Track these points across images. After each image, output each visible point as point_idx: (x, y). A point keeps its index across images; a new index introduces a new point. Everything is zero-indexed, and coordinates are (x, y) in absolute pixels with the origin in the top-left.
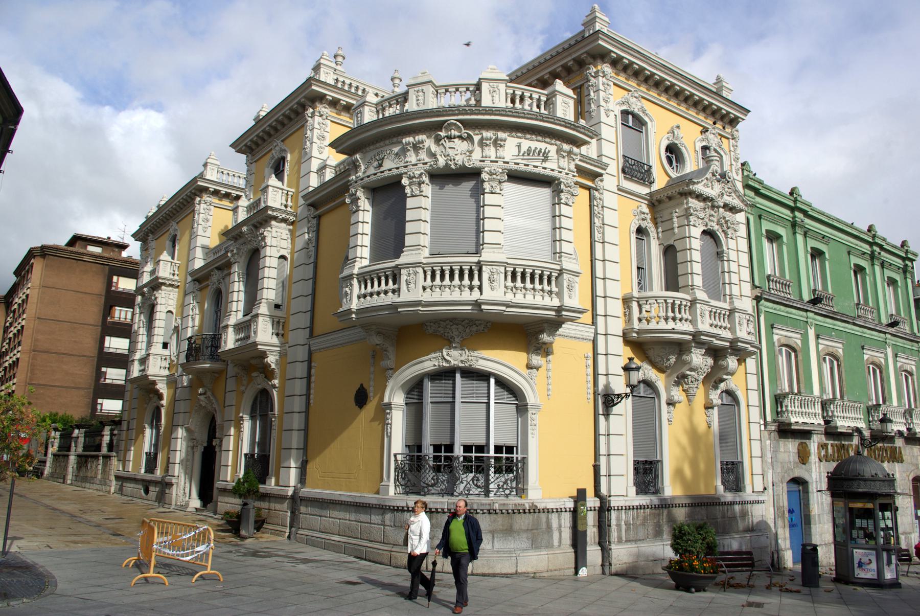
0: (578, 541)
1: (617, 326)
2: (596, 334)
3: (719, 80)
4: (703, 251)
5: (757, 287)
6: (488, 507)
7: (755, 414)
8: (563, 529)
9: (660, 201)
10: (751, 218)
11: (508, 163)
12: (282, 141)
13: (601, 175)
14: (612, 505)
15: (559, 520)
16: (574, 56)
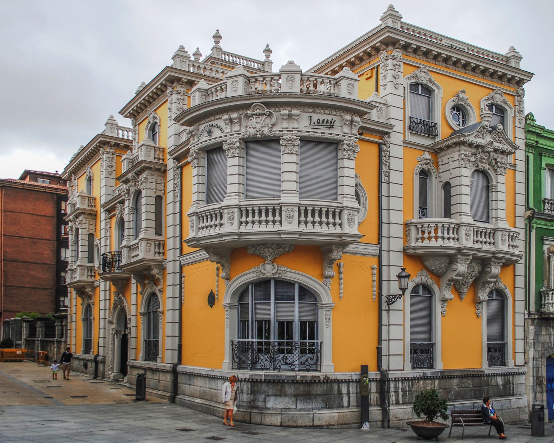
0: (363, 403)
1: (397, 244)
2: (381, 251)
3: (513, 49)
4: (472, 186)
5: (530, 209)
6: (292, 378)
7: (520, 306)
8: (351, 395)
10: (531, 156)
11: (301, 131)
12: (155, 110)
13: (389, 133)
14: (390, 376)
15: (348, 388)
16: (371, 44)
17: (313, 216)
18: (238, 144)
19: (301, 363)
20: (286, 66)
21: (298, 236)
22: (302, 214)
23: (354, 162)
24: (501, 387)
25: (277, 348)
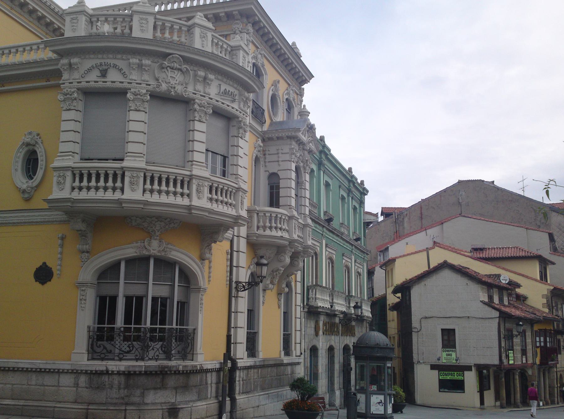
6: (174, 369)
7: (299, 302)
9: (271, 139)
11: (211, 99)
16: (226, 10)
17: (160, 184)
19: (179, 351)
22: (148, 181)
25: (148, 335)
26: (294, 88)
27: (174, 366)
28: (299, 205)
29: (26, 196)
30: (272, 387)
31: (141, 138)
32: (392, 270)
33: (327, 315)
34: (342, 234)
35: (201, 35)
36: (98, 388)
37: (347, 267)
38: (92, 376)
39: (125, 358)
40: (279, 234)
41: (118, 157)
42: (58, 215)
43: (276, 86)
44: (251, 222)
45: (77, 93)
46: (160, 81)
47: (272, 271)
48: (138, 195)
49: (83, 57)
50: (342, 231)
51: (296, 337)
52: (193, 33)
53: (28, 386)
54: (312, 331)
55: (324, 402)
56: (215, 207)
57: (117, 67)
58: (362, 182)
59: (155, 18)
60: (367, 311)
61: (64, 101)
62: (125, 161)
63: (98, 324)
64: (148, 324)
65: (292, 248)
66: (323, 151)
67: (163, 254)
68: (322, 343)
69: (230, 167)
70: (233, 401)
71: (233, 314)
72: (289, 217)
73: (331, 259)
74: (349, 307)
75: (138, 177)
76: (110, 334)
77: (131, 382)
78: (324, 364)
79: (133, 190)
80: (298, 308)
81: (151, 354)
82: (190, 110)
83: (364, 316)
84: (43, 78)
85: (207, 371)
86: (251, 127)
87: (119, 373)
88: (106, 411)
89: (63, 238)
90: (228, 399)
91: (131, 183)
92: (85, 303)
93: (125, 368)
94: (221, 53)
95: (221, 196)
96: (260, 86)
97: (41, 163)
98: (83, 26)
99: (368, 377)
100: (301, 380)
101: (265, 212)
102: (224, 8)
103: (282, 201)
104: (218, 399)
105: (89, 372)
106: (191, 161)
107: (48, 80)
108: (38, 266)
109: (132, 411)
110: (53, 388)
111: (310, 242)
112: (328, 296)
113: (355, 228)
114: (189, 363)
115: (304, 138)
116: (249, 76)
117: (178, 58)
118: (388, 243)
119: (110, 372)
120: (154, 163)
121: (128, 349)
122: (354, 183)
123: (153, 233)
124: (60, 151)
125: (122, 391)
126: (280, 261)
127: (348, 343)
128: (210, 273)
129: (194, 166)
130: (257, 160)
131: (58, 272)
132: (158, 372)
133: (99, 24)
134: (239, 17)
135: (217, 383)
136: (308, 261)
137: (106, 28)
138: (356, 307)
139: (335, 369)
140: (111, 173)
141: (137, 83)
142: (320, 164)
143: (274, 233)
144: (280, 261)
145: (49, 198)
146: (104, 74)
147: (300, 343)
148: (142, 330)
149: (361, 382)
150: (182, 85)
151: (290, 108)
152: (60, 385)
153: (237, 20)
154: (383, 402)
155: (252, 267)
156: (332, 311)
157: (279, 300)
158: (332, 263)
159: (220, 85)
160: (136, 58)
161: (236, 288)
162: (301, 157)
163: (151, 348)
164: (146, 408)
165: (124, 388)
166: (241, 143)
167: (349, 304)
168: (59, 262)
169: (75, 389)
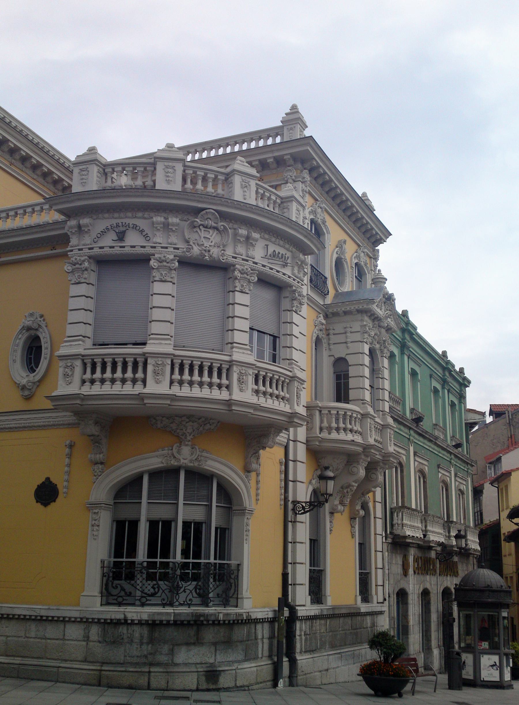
6: (213, 618)
7: (380, 529)
11: (256, 263)
18: (86, 264)
19: (218, 595)
20: (163, 150)
21: (168, 402)
22: (177, 370)
23: (248, 296)
24: (369, 629)
25: (178, 572)
26: (366, 250)
27: (212, 615)
28: (375, 400)
29: (26, 393)
30: (345, 645)
31: (168, 315)
32: (507, 487)
33: (419, 547)
34: (437, 438)
35: (242, 185)
36: (114, 642)
37: (444, 482)
38: (106, 626)
39: (148, 602)
40: (350, 437)
41: (139, 340)
42: (67, 417)
43: (341, 247)
44: (312, 423)
45: (88, 261)
46: (191, 243)
47: (342, 488)
48: (163, 388)
49: (95, 217)
50: (436, 434)
51: (377, 577)
52: (232, 183)
53: (26, 639)
54: (399, 570)
55: (416, 665)
56: (262, 401)
57: (138, 228)
58: (462, 370)
59: (185, 166)
60: (473, 542)
61: (72, 272)
62: (148, 345)
63: (115, 557)
64: (179, 558)
65: (367, 456)
66: (406, 329)
67: (196, 464)
68: (413, 586)
69: (282, 350)
70: (293, 662)
71: (290, 545)
72: (362, 415)
73: (422, 473)
74: (449, 537)
75: (164, 365)
76: (129, 570)
77: (156, 635)
78: (417, 614)
79: (158, 382)
80: (379, 538)
81: (182, 597)
82: (229, 279)
83: (470, 549)
84: (48, 245)
85: (257, 621)
86: (310, 299)
87: (141, 623)
88: (123, 674)
89: (71, 446)
90: (285, 659)
91: (156, 373)
92: (98, 530)
93: (149, 615)
94: (268, 206)
95: (271, 387)
96: (319, 246)
97: (45, 352)
98: (95, 178)
99: (477, 630)
100: (384, 635)
101: (330, 409)
102: (272, 151)
103: (352, 394)
104: (272, 659)
105: (103, 621)
106: (231, 343)
107: (54, 248)
108: (40, 482)
109: (158, 674)
110: (57, 642)
111: (391, 449)
112: (419, 521)
113: (454, 431)
114: (232, 610)
115: (381, 312)
116: (305, 233)
117: (213, 214)
118: (500, 452)
119: (129, 622)
120: (184, 347)
121: (152, 590)
122: (450, 371)
123: (183, 437)
124: (67, 335)
125: (144, 647)
126: (352, 474)
127: (449, 586)
128: (257, 489)
129: (234, 349)
130: (318, 342)
131: (65, 490)
132: (192, 622)
133: (114, 175)
134: (291, 162)
135: (271, 638)
136: (391, 474)
137: (124, 181)
138: (458, 537)
139: (432, 621)
140: (130, 360)
141: (162, 247)
142: (403, 347)
143: (342, 436)
144: (352, 474)
145: (54, 394)
146: (121, 237)
147: (383, 586)
148: (171, 564)
149: (468, 637)
150: (218, 247)
151: (360, 275)
152: (66, 638)
153: (289, 166)
154: (498, 664)
155: (314, 482)
156: (425, 542)
157: (352, 527)
158: (424, 477)
159: (267, 245)
160: (161, 216)
161: (293, 510)
162: (376, 337)
163: (182, 590)
164: (175, 670)
165: (148, 644)
166: (296, 318)
167: (449, 532)
168: (66, 477)
169: (84, 643)
